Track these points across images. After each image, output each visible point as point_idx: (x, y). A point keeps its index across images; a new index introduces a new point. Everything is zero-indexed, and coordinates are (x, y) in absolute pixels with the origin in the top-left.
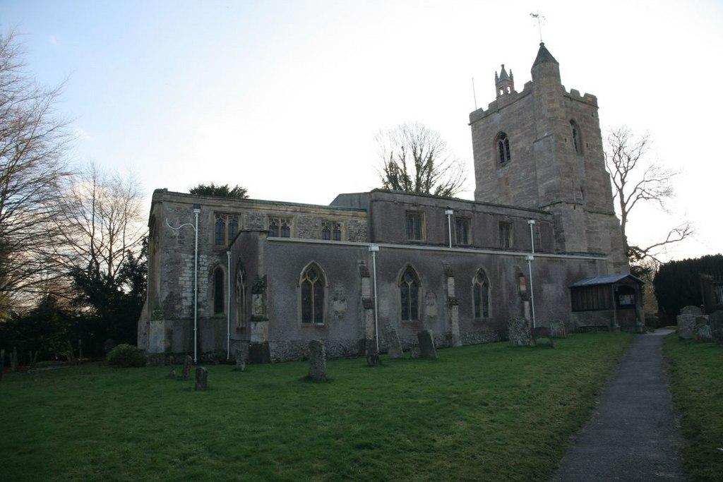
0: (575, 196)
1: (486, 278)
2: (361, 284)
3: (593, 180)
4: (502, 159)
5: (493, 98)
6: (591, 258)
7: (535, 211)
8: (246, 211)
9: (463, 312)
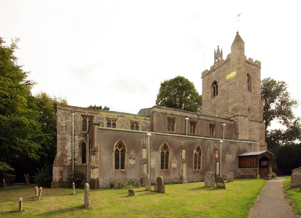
0: (246, 112)
1: (200, 151)
2: (142, 152)
3: (255, 105)
4: (214, 95)
6: (250, 142)
7: (227, 119)
9: (189, 166)
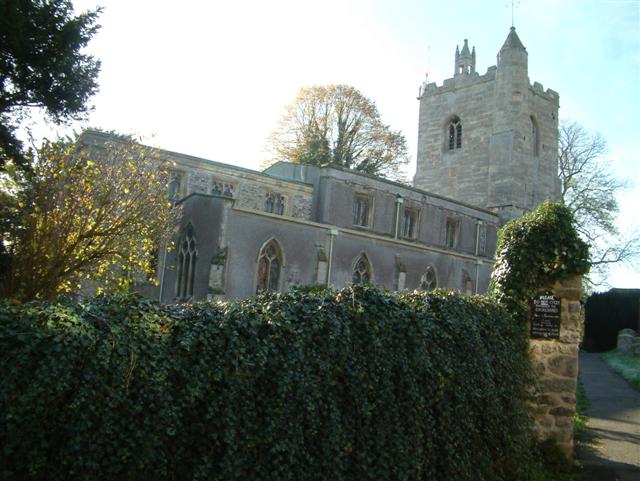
5: (450, 74)
8: (190, 169)
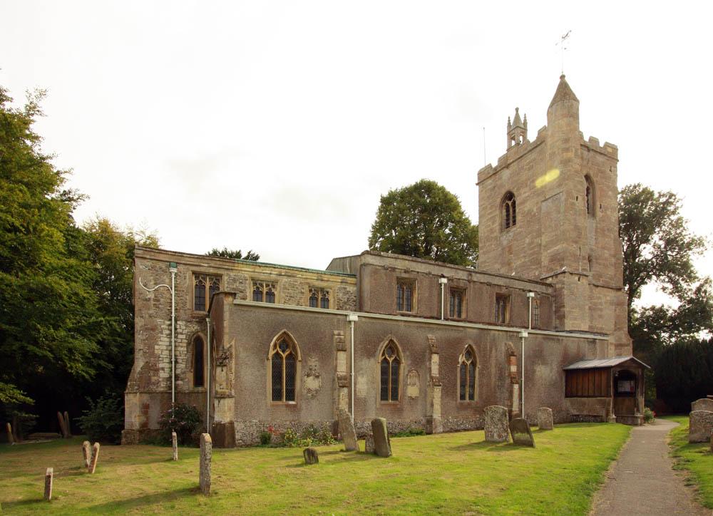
0: (582, 266)
1: (475, 357)
2: (336, 359)
3: (604, 248)
4: (508, 225)
6: (592, 336)
7: (537, 283)
9: (448, 392)
